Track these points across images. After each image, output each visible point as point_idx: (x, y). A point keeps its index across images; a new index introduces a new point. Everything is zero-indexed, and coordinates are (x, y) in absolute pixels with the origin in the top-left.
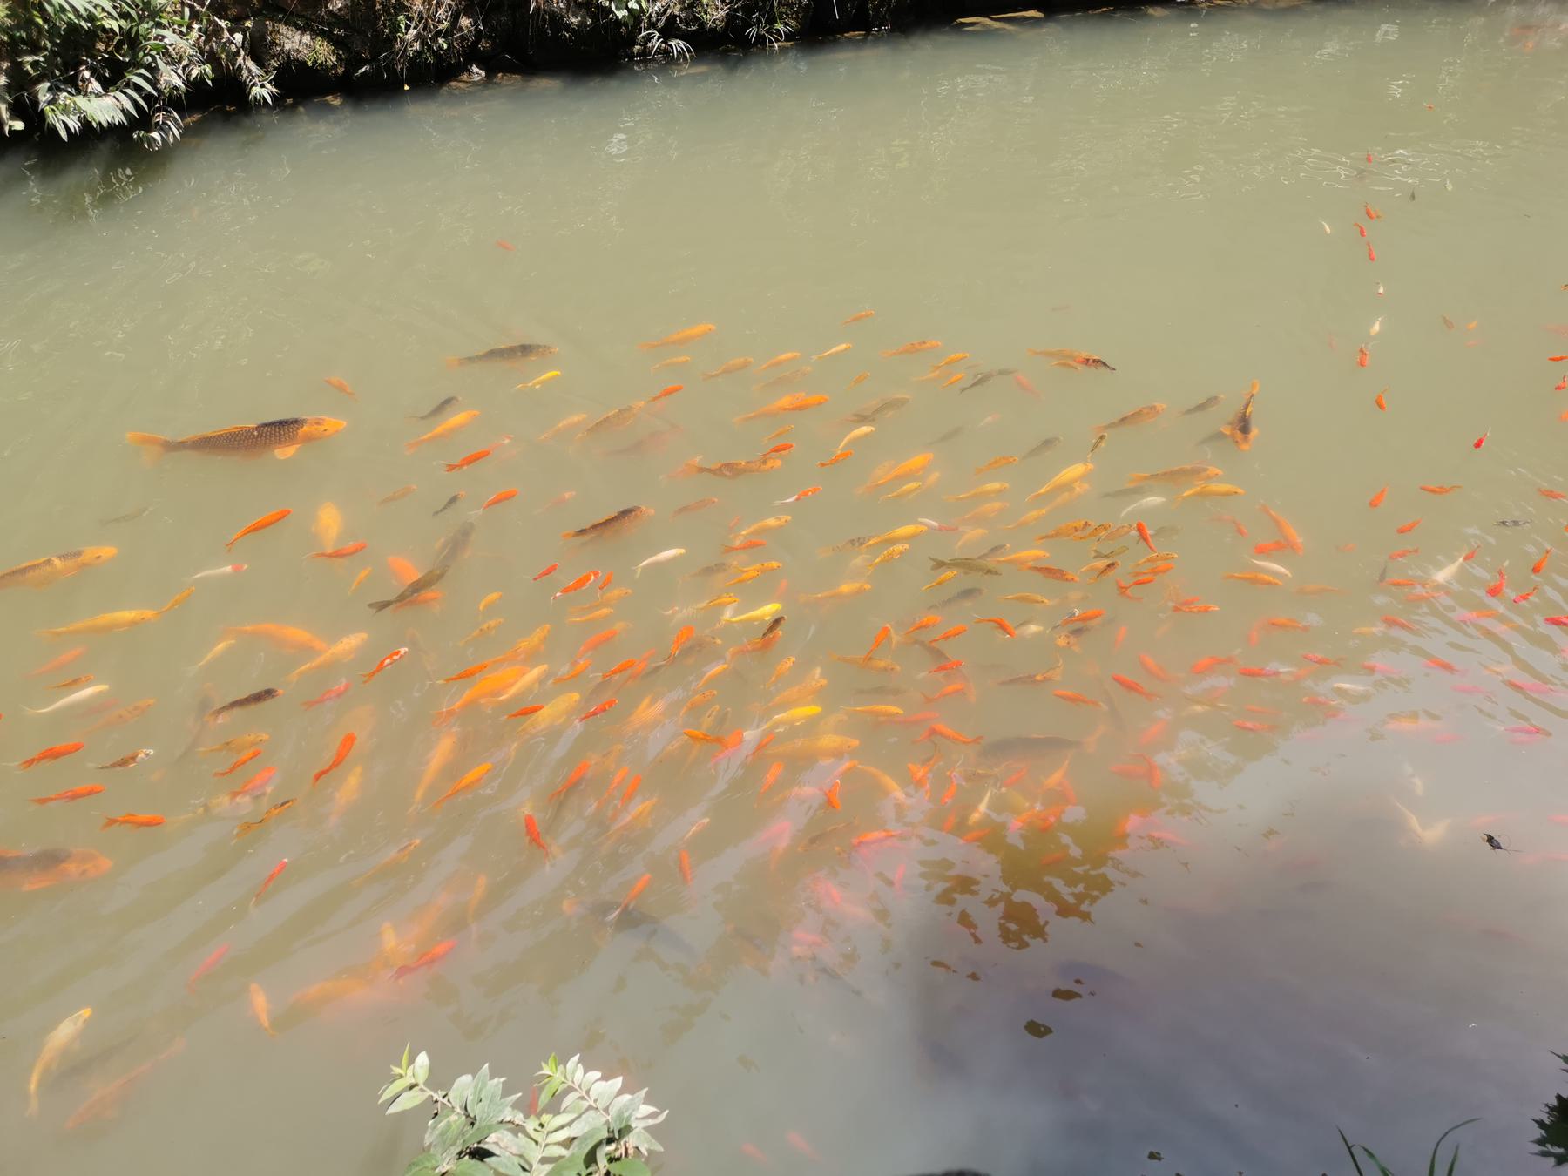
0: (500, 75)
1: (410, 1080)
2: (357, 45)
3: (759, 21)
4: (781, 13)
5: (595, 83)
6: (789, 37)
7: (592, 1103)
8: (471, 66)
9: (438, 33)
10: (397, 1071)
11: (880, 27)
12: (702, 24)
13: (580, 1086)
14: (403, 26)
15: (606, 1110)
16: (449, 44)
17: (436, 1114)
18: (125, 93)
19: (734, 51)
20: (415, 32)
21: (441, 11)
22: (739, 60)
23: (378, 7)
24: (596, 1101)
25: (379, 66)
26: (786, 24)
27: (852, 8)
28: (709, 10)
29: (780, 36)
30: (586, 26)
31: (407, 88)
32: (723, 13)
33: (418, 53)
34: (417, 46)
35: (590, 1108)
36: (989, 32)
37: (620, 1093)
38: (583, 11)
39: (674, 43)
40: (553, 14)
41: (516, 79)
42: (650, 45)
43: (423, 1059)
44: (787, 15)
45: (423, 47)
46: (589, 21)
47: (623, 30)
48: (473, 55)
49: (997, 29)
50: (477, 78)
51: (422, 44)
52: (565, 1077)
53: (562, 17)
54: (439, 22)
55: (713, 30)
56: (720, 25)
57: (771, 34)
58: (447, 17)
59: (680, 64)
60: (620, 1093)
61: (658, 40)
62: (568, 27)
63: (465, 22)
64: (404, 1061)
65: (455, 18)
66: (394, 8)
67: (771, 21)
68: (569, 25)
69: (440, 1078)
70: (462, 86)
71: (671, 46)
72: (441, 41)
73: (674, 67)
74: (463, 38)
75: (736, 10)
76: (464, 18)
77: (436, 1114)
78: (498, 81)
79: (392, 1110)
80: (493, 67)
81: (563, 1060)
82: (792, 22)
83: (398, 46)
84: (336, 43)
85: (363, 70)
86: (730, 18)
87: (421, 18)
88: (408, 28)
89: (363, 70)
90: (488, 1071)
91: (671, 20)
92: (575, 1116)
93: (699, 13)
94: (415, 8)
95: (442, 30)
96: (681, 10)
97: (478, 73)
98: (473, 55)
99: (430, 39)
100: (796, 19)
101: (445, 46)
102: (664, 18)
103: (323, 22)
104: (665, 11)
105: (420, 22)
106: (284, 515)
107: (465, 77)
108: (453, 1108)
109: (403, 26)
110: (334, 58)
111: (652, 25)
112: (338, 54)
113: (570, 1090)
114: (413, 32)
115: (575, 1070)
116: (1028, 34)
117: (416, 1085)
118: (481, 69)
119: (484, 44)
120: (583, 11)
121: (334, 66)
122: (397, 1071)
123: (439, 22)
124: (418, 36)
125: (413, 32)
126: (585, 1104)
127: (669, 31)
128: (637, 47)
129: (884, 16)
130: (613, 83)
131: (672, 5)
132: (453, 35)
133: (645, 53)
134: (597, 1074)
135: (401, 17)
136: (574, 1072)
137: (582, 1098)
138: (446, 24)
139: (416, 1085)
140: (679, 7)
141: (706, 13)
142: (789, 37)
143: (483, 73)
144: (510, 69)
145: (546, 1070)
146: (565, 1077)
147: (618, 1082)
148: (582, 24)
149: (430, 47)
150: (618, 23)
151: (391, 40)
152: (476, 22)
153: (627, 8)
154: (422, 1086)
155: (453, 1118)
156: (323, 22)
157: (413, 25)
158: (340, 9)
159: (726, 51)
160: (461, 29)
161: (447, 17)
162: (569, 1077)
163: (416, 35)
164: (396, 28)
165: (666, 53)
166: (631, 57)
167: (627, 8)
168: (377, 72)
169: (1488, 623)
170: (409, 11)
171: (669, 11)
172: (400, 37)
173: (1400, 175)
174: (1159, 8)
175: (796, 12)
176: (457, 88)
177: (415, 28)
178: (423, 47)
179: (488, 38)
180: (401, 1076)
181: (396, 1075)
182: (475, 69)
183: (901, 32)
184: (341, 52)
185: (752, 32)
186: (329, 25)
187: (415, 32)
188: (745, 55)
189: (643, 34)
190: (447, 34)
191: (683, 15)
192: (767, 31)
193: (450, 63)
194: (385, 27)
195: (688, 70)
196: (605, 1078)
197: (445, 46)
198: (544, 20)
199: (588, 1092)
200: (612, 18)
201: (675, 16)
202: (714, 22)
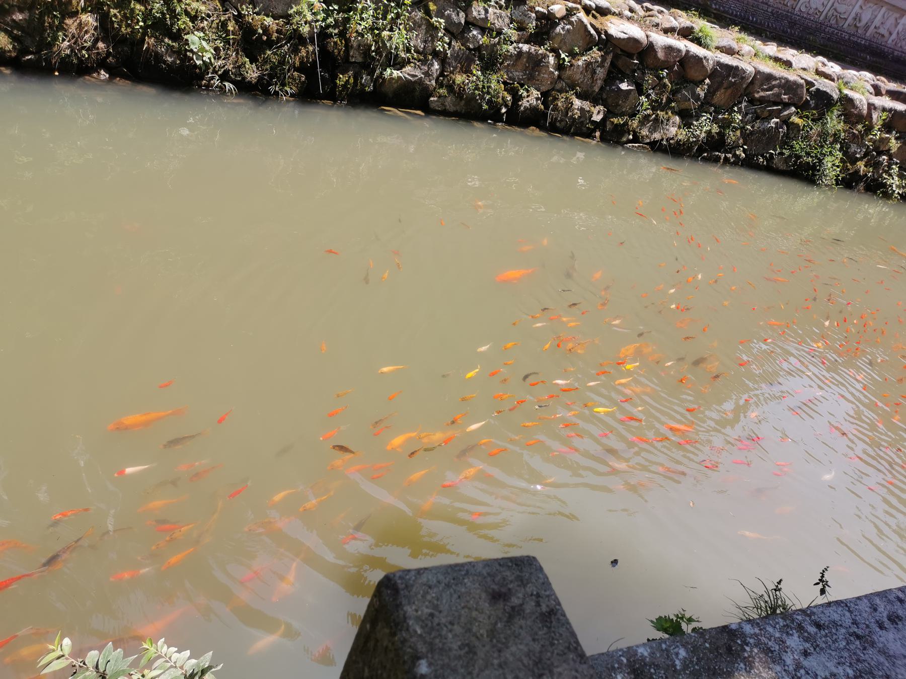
0: (118, 79)
1: (59, 653)
2: (28, 41)
3: (276, 84)
4: (289, 82)
5: (176, 95)
6: (292, 95)
7: (173, 664)
8: (101, 70)
9: (83, 48)
10: (51, 647)
11: (341, 101)
12: (244, 78)
13: (165, 655)
14: (61, 39)
15: (182, 668)
16: (89, 55)
17: (75, 673)
18: (872, 448)
19: (260, 96)
20: (68, 44)
21: (86, 37)
22: (264, 102)
23: (46, 24)
24: (175, 663)
25: (40, 57)
26: (291, 89)
27: (328, 88)
28: (249, 72)
29: (288, 94)
30: (176, 64)
31: (57, 73)
32: (257, 75)
33: (68, 56)
34: (68, 52)
35: (171, 667)
36: (396, 117)
37: (189, 658)
38: (175, 56)
39: (227, 84)
40: (157, 53)
41: (128, 83)
42: (212, 82)
43: (67, 642)
44: (292, 84)
45: (72, 53)
46: (178, 62)
47: (198, 71)
48: (102, 64)
49: (401, 116)
50: (102, 77)
51: (72, 51)
52: (157, 650)
53: (162, 56)
54: (85, 41)
55: (250, 82)
56: (254, 81)
57: (282, 91)
58: (90, 40)
59: (228, 96)
60: (189, 658)
61: (218, 80)
62: (165, 62)
63: (101, 45)
64: (56, 642)
65: (96, 41)
66: (57, 27)
67: (283, 85)
68: (166, 61)
69: (79, 652)
70: (93, 80)
71: (225, 85)
72: (84, 52)
73: (225, 97)
74: (98, 54)
75: (265, 75)
76: (101, 43)
77: (75, 673)
78: (117, 82)
79: (47, 671)
80: (114, 73)
81: (154, 641)
82: (294, 88)
83: (55, 49)
84: (14, 38)
85: (30, 57)
86: (260, 78)
87: (73, 37)
88: (64, 40)
89: (30, 57)
90: (112, 646)
91: (226, 72)
92: (162, 671)
93: (243, 71)
94: (70, 30)
95: (86, 47)
96: (233, 68)
97: (104, 75)
98: (102, 64)
99: (78, 50)
100: (297, 87)
101: (87, 56)
102: (223, 70)
103: (8, 25)
104: (224, 66)
105: (72, 39)
106: (829, 486)
107: (95, 75)
108: (88, 668)
109: (61, 39)
110: (11, 47)
111: (215, 72)
112: (14, 45)
113: (160, 657)
114: (66, 43)
115: (162, 647)
116: (418, 122)
117: (63, 656)
118: (106, 73)
119: (110, 59)
120: (175, 56)
121: (10, 51)
122: (51, 647)
123: (85, 41)
124: (70, 46)
125: (66, 43)
126: (169, 665)
127: (224, 77)
128: (204, 81)
129: (344, 97)
130: (187, 98)
131: (228, 64)
132: (92, 51)
133: (208, 86)
134: (174, 649)
135: (60, 33)
136: (162, 647)
137: (167, 662)
138: (89, 44)
139: (63, 656)
140: (232, 66)
141: (247, 73)
142: (292, 95)
143: (107, 76)
144: (124, 76)
145: (145, 646)
146: (157, 650)
147: (187, 653)
148: (174, 62)
149: (76, 54)
150: (195, 66)
151: (50, 46)
152: (108, 47)
153: (202, 60)
154: (67, 656)
155: (88, 673)
156: (8, 25)
157: (68, 39)
158: (20, 20)
159: (256, 95)
160: (98, 49)
161: (90, 40)
162: (159, 650)
163: (68, 45)
164: (55, 38)
165: (222, 89)
166: (200, 86)
167: (202, 60)
168: (39, 61)
169: (688, 455)
170: (66, 31)
171: (226, 67)
172: (58, 45)
173: (793, 355)
174: (479, 123)
175: (298, 84)
176: (89, 80)
177: (68, 41)
178: (72, 53)
179: (114, 57)
180: (54, 651)
181: (51, 650)
182: (102, 72)
183: (352, 106)
184: (16, 44)
185: (272, 89)
186: (11, 27)
187: (68, 44)
188: (266, 99)
189: (210, 75)
190: (88, 49)
191: (233, 71)
192: (280, 90)
193: (87, 66)
194: (49, 37)
195: (233, 100)
196: (179, 652)
197: (87, 56)
198: (151, 55)
199: (170, 658)
200: (192, 63)
201: (229, 70)
202: (251, 78)
